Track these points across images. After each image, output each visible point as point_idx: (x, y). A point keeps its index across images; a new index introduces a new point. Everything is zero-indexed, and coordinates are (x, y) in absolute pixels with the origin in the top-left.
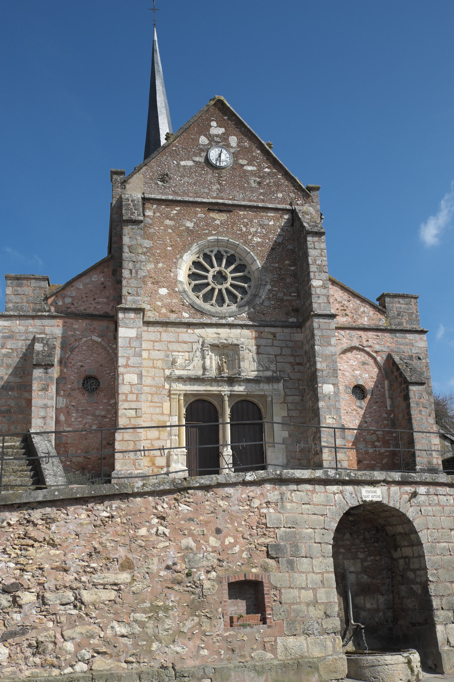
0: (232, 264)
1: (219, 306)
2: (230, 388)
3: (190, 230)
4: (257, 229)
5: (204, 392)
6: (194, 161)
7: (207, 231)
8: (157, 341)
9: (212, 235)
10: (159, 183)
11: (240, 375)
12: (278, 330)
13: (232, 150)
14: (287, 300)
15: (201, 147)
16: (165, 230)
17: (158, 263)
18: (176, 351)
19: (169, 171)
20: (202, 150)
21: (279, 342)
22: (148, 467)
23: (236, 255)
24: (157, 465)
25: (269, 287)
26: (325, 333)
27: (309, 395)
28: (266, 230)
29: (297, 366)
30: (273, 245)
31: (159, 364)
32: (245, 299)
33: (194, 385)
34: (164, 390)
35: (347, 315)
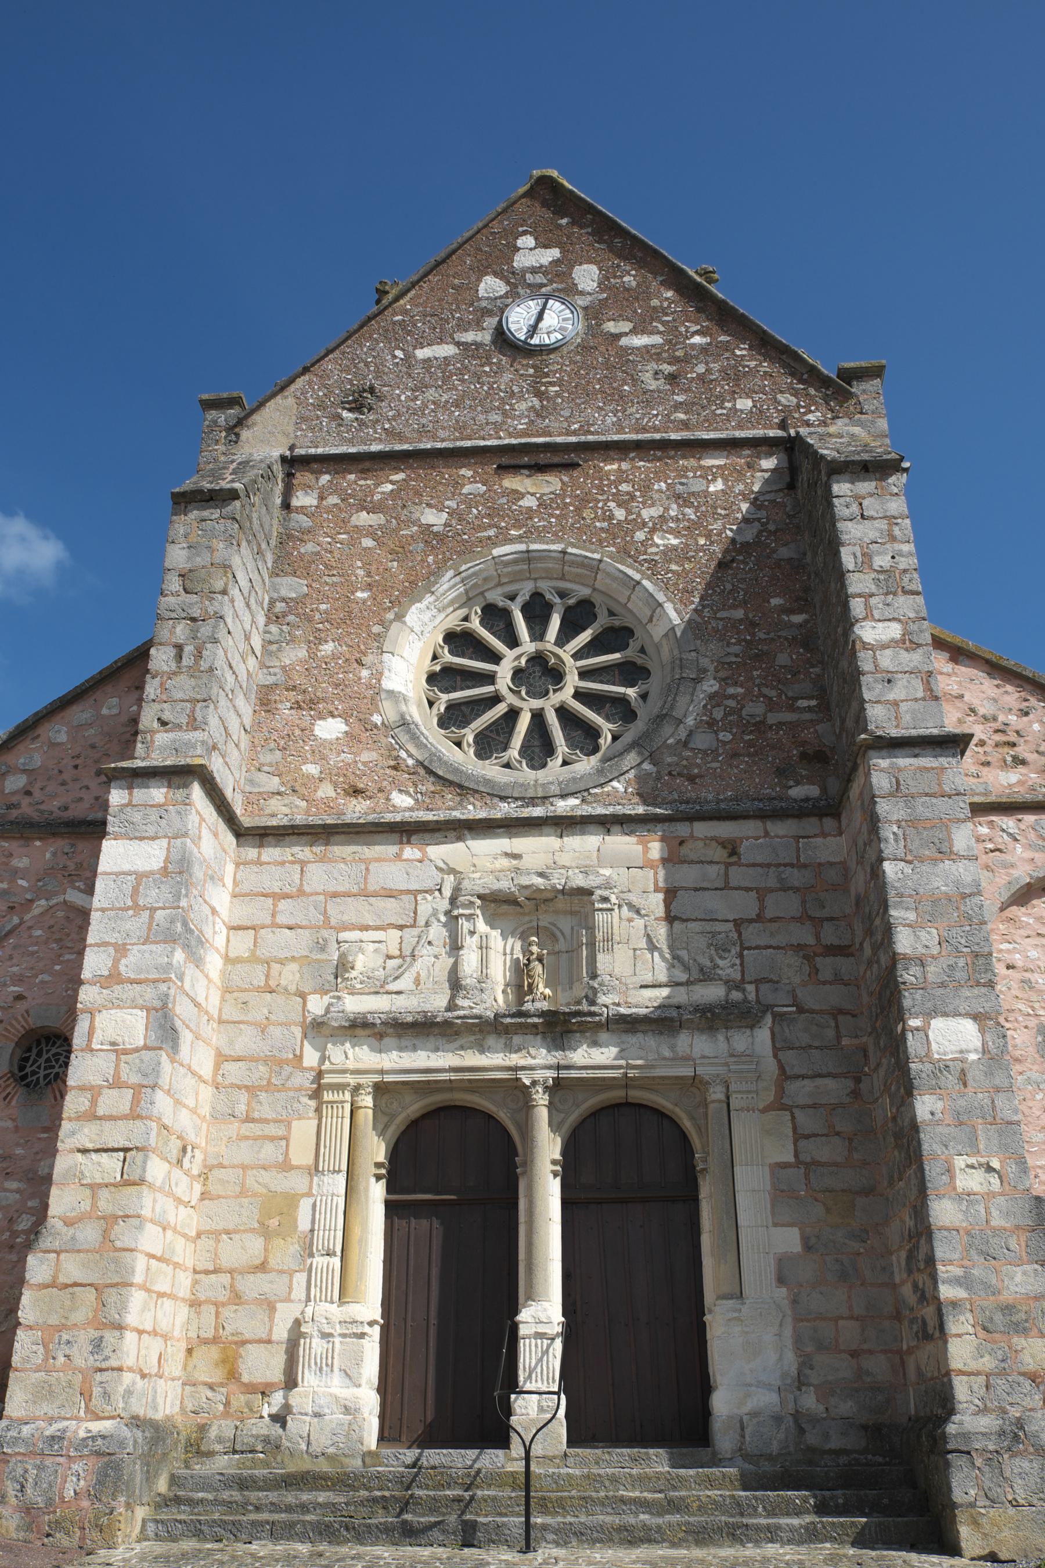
0: (584, 629)
1: (532, 767)
3: (436, 534)
4: (667, 509)
5: (453, 1076)
6: (458, 344)
7: (492, 532)
8: (287, 896)
9: (511, 541)
10: (345, 414)
11: (593, 1003)
12: (749, 828)
13: (582, 301)
14: (780, 724)
15: (484, 304)
16: (353, 542)
17: (321, 641)
18: (353, 927)
19: (376, 378)
20: (487, 312)
22: (211, 1387)
23: (597, 599)
24: (245, 1378)
25: (710, 686)
26: (922, 808)
27: (882, 1072)
28: (697, 509)
29: (829, 960)
30: (726, 551)
31: (289, 976)
32: (627, 738)
33: (415, 1049)
35: (1023, 762)
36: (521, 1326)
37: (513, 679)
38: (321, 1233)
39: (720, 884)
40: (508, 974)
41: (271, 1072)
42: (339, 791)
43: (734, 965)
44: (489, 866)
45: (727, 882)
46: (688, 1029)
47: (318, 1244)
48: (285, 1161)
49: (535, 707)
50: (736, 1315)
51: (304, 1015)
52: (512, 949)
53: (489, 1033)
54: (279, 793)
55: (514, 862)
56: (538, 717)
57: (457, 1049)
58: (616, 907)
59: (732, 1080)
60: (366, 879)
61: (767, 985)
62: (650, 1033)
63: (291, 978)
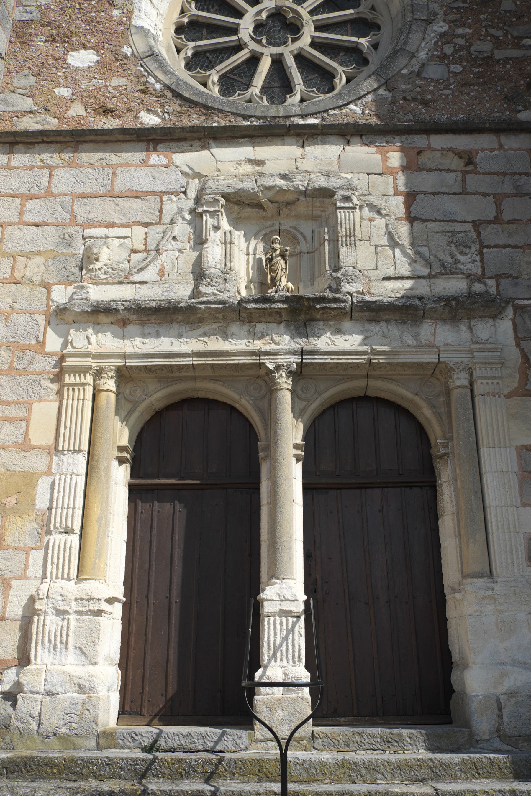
2: (302, 343)
5: (196, 361)
11: (338, 291)
14: (507, 59)
21: (487, 178)
25: (440, 27)
33: (158, 335)
34: (40, 357)
36: (265, 603)
37: (254, 31)
38: (59, 511)
39: (459, 189)
40: (251, 272)
41: (13, 357)
42: (89, 110)
43: (474, 261)
44: (233, 171)
45: (464, 187)
46: (431, 319)
47: (56, 521)
48: (25, 441)
49: (275, 53)
50: (489, 593)
51: (48, 304)
52: (255, 249)
53: (232, 320)
54: (31, 112)
55: (258, 168)
56: (278, 62)
57: (200, 336)
58: (358, 207)
59: (477, 366)
60: (112, 182)
61: (507, 280)
62: (393, 322)
63: (36, 270)
